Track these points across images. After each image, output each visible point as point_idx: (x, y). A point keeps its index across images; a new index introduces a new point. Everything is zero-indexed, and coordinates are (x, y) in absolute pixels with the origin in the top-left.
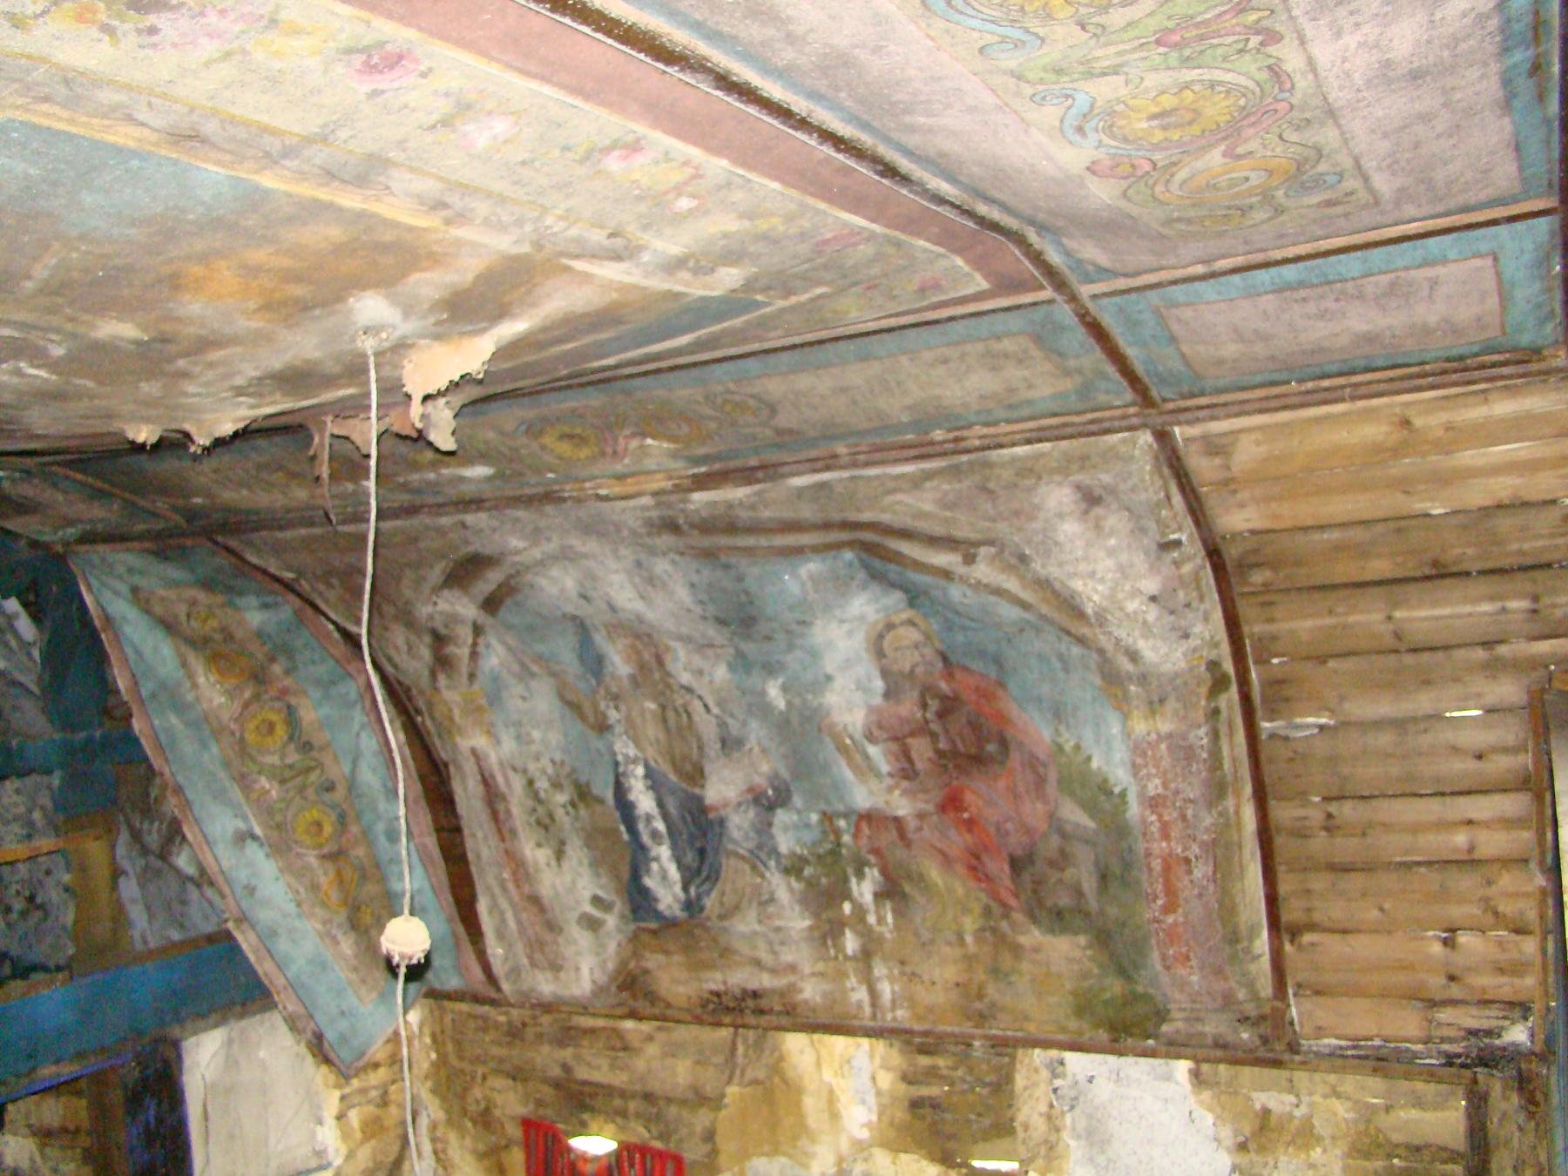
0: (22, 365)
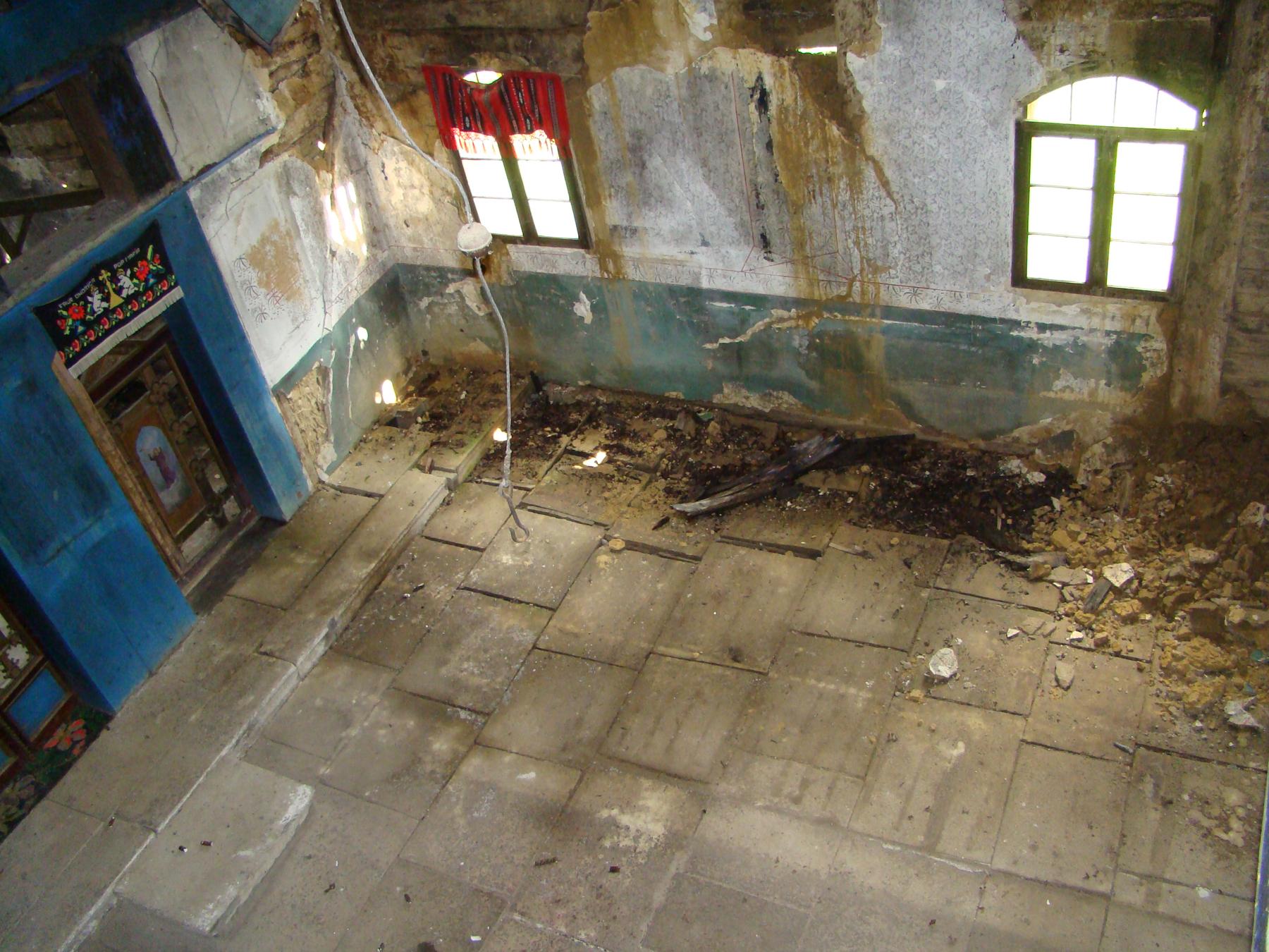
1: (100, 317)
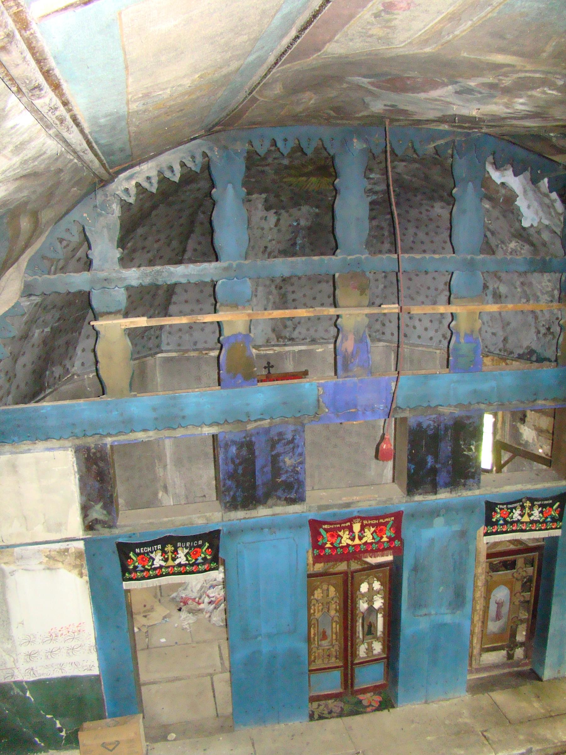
1: (514, 522)
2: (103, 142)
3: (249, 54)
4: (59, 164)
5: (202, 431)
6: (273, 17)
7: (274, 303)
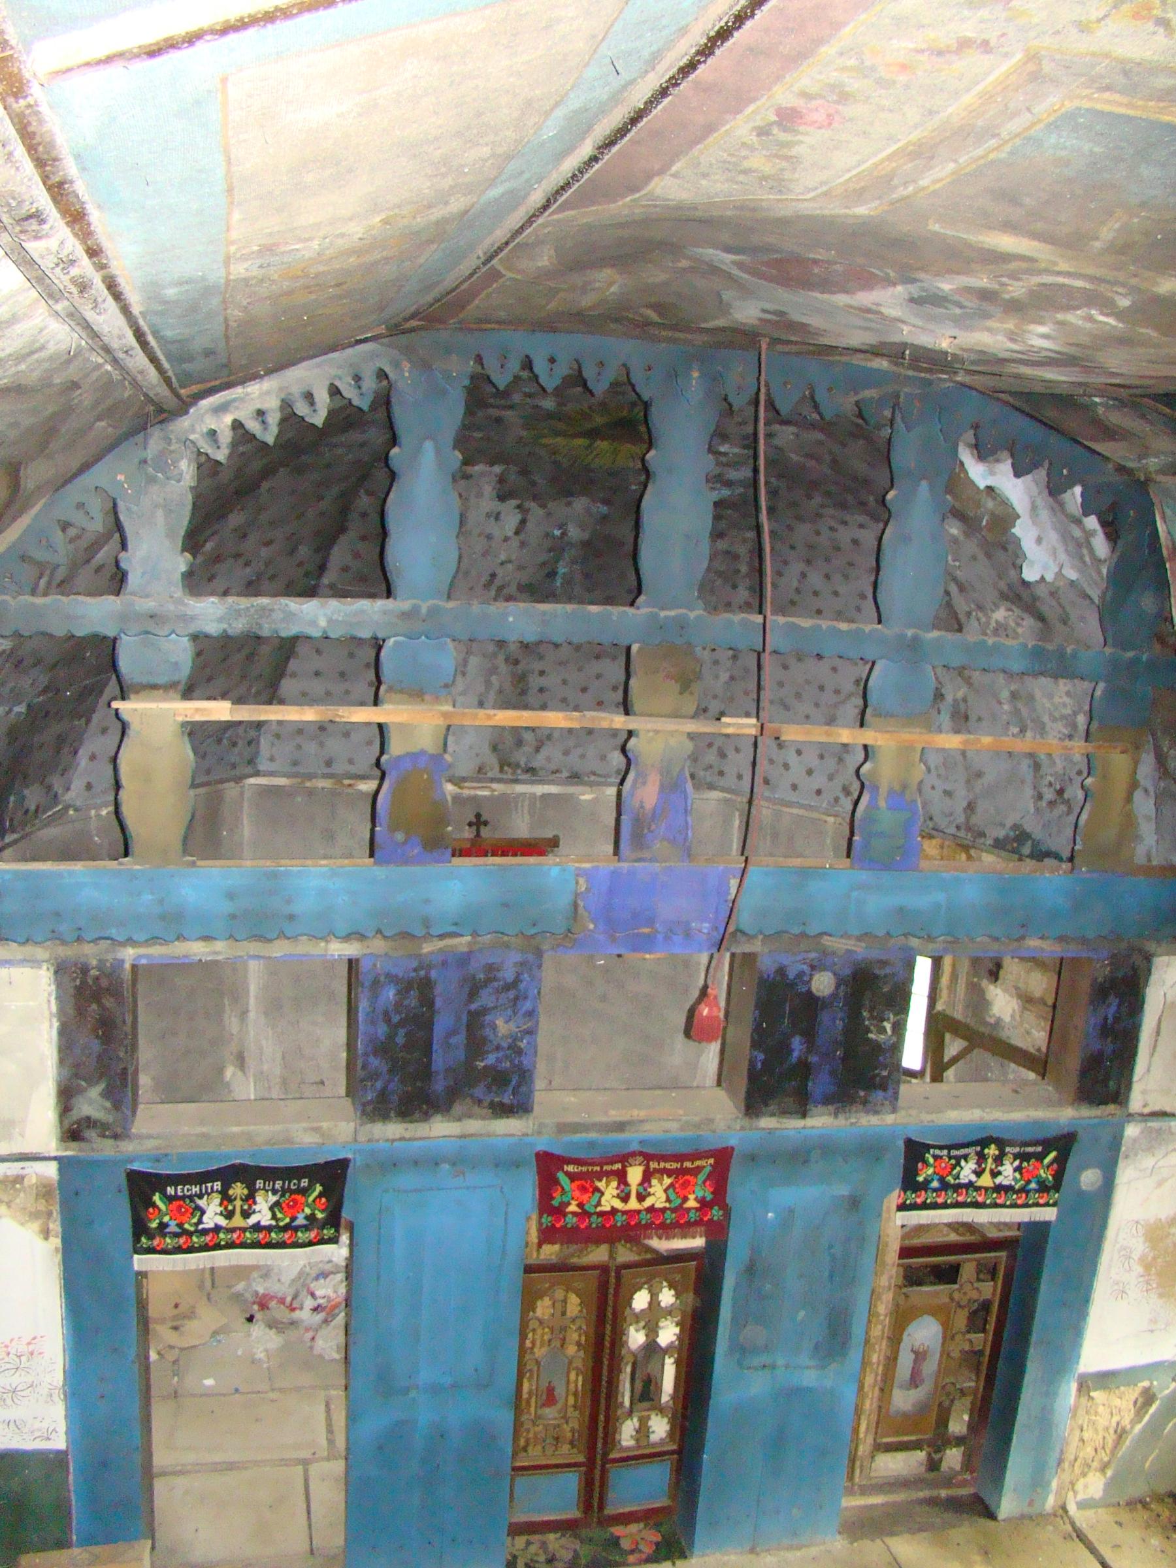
0: (1093, 312)
1: (960, 1186)
2: (169, 333)
3: (492, 182)
4: (72, 372)
5: (326, 950)
6: (547, 114)
7: (500, 692)
